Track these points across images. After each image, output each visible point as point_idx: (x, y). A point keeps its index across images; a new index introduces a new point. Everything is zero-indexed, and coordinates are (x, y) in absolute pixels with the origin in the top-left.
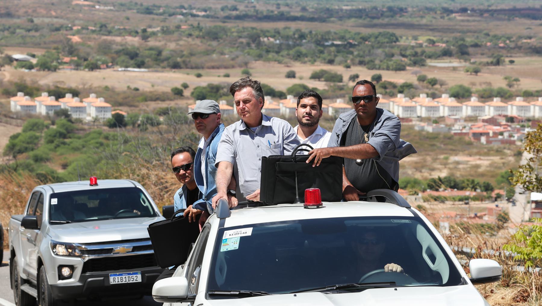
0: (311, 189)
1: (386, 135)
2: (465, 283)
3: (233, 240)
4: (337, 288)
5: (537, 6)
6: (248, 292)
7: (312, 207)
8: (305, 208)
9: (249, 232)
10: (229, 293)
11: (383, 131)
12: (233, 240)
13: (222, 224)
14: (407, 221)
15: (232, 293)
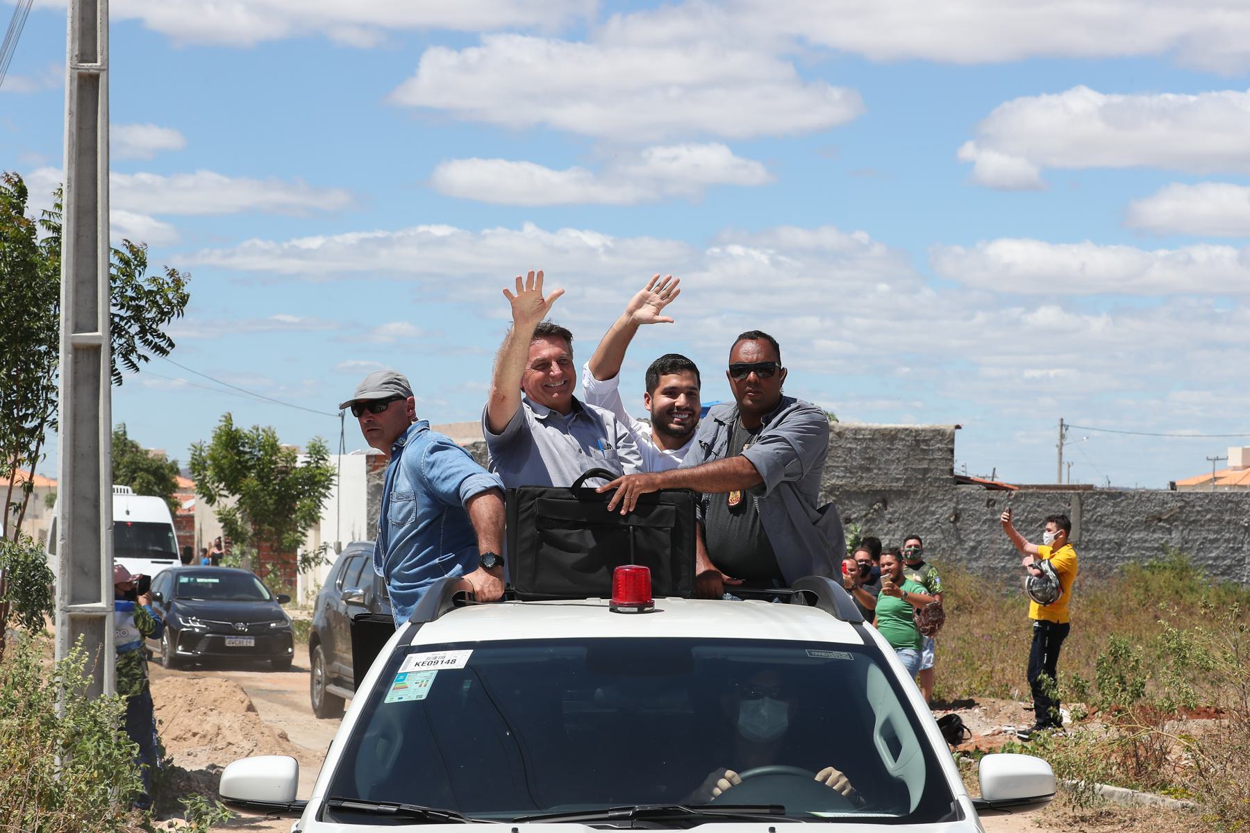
0: (627, 568)
1: (784, 440)
2: (958, 815)
3: (418, 677)
4: (636, 815)
5: (1233, 472)
6: (418, 808)
7: (628, 609)
8: (611, 610)
9: (461, 659)
10: (374, 808)
11: (782, 431)
12: (418, 677)
13: (410, 635)
14: (844, 655)
15: (381, 807)
